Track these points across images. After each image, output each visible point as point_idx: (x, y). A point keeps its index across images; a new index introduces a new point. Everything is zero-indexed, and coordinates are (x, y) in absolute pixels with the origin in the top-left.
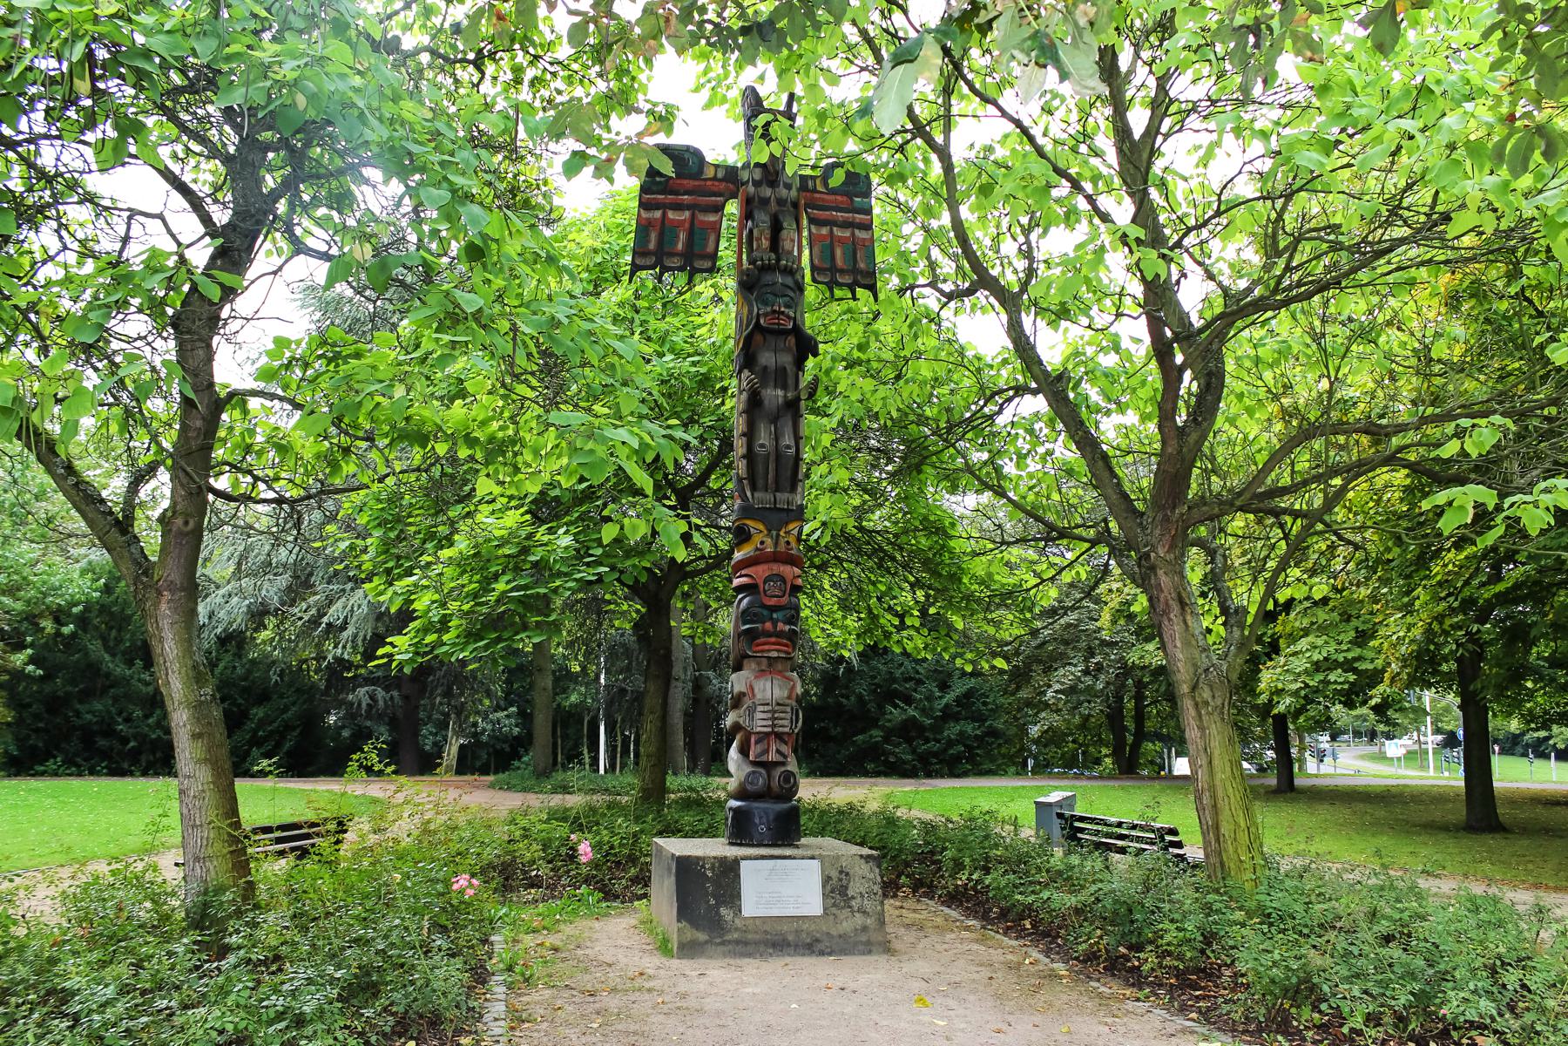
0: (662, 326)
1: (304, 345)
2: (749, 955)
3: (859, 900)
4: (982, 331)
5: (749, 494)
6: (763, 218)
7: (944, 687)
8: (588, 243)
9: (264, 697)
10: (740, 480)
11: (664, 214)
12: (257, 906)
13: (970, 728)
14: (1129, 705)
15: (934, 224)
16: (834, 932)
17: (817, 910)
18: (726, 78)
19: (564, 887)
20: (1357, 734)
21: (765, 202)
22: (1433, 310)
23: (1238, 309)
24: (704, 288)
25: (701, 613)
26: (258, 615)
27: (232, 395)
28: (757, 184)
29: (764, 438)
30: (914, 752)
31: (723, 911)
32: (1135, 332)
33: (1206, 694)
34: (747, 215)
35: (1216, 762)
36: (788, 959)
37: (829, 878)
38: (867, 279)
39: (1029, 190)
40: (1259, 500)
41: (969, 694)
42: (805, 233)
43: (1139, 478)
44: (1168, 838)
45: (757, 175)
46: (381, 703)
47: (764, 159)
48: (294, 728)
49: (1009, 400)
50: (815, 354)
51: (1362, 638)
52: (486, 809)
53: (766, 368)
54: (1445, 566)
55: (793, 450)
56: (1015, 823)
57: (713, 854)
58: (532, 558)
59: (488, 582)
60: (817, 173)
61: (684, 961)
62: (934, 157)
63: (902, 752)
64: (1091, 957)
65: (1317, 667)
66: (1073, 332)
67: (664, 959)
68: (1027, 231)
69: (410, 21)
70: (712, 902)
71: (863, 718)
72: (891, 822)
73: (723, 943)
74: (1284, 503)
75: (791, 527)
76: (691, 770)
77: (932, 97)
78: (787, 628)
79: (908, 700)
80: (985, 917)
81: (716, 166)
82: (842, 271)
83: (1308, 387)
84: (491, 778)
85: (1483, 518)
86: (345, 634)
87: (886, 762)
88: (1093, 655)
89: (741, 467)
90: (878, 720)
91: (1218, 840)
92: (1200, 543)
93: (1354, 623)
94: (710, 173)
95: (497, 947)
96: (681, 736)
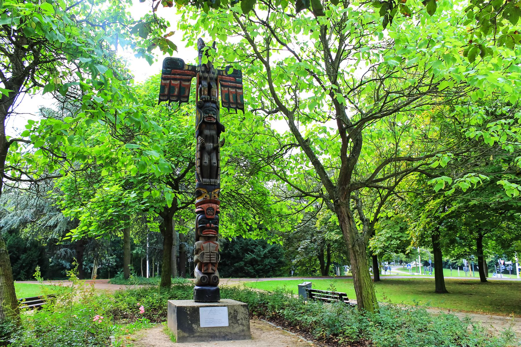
0: (170, 122)
1: (39, 123)
2: (203, 341)
3: (241, 321)
4: (280, 125)
5: (201, 179)
6: (205, 83)
7: (264, 247)
8: (143, 93)
9: (25, 250)
10: (198, 174)
11: (170, 82)
12: (22, 328)
13: (273, 261)
14: (326, 253)
15: (263, 88)
16: (233, 332)
18: (193, 36)
19: (136, 318)
20: (396, 262)
21: (205, 79)
22: (427, 120)
23: (367, 118)
24: (184, 107)
25: (182, 223)
26: (24, 223)
27: (12, 141)
28: (203, 72)
29: (206, 160)
30: (254, 269)
31: (194, 325)
32: (333, 125)
33: (357, 248)
34: (199, 83)
35: (361, 271)
36: (217, 342)
38: (240, 105)
39: (299, 72)
40: (371, 182)
41: (272, 249)
42: (220, 91)
43: (334, 176)
44: (343, 297)
45: (203, 69)
46: (69, 254)
47: (206, 62)
49: (290, 148)
50: (224, 131)
51: (402, 230)
52: (102, 292)
53: (206, 135)
54: (429, 206)
55: (216, 164)
56: (292, 293)
57: (190, 305)
58: (122, 202)
59: (106, 210)
60: (224, 69)
61: (180, 344)
62: (264, 66)
63: (250, 269)
64: (320, 339)
65: (388, 239)
66: (312, 125)
67: (173, 343)
68: (295, 91)
69: (79, 11)
70: (190, 322)
71: (238, 258)
72: (249, 293)
73: (194, 337)
74: (380, 184)
75: (216, 191)
76: (179, 275)
77: (263, 45)
79: (252, 252)
80: (283, 325)
81: (189, 66)
82: (232, 103)
83: (387, 146)
84: (109, 280)
85: (448, 187)
86: (56, 229)
87: (245, 273)
88: (313, 236)
89: (198, 170)
90: (242, 258)
91: (362, 298)
92: (353, 197)
93: (400, 225)
94: (186, 68)
95: (112, 341)
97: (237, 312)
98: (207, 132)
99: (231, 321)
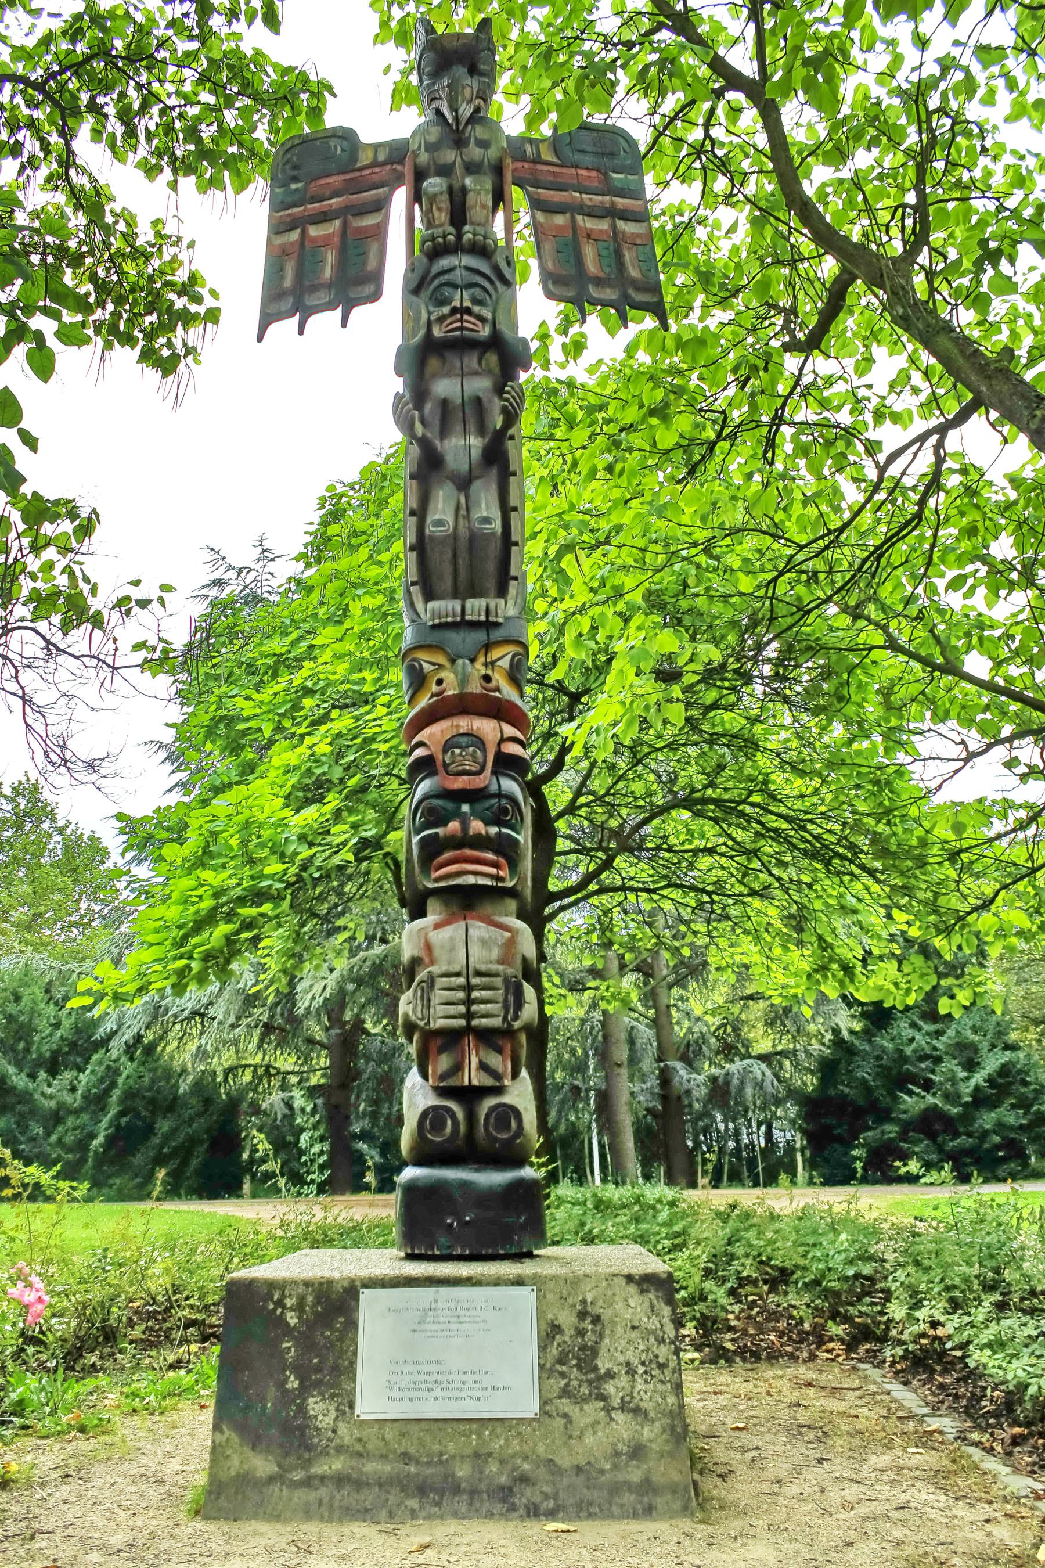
2: (364, 1514)
3: (623, 1381)
5: (419, 606)
7: (971, 1066)
9: (172, 1105)
11: (304, 233)
13: (1012, 1118)
16: (565, 1461)
17: (523, 1402)
29: (443, 508)
36: (452, 1526)
37: (556, 1328)
41: (1004, 1070)
48: (201, 1142)
55: (497, 526)
70: (293, 1383)
75: (495, 654)
78: (493, 830)
79: (928, 1086)
81: (376, 147)
82: (598, 282)
94: (365, 158)
96: (875, 1203)
97: (597, 1319)
98: (445, 387)
99: (557, 1384)
